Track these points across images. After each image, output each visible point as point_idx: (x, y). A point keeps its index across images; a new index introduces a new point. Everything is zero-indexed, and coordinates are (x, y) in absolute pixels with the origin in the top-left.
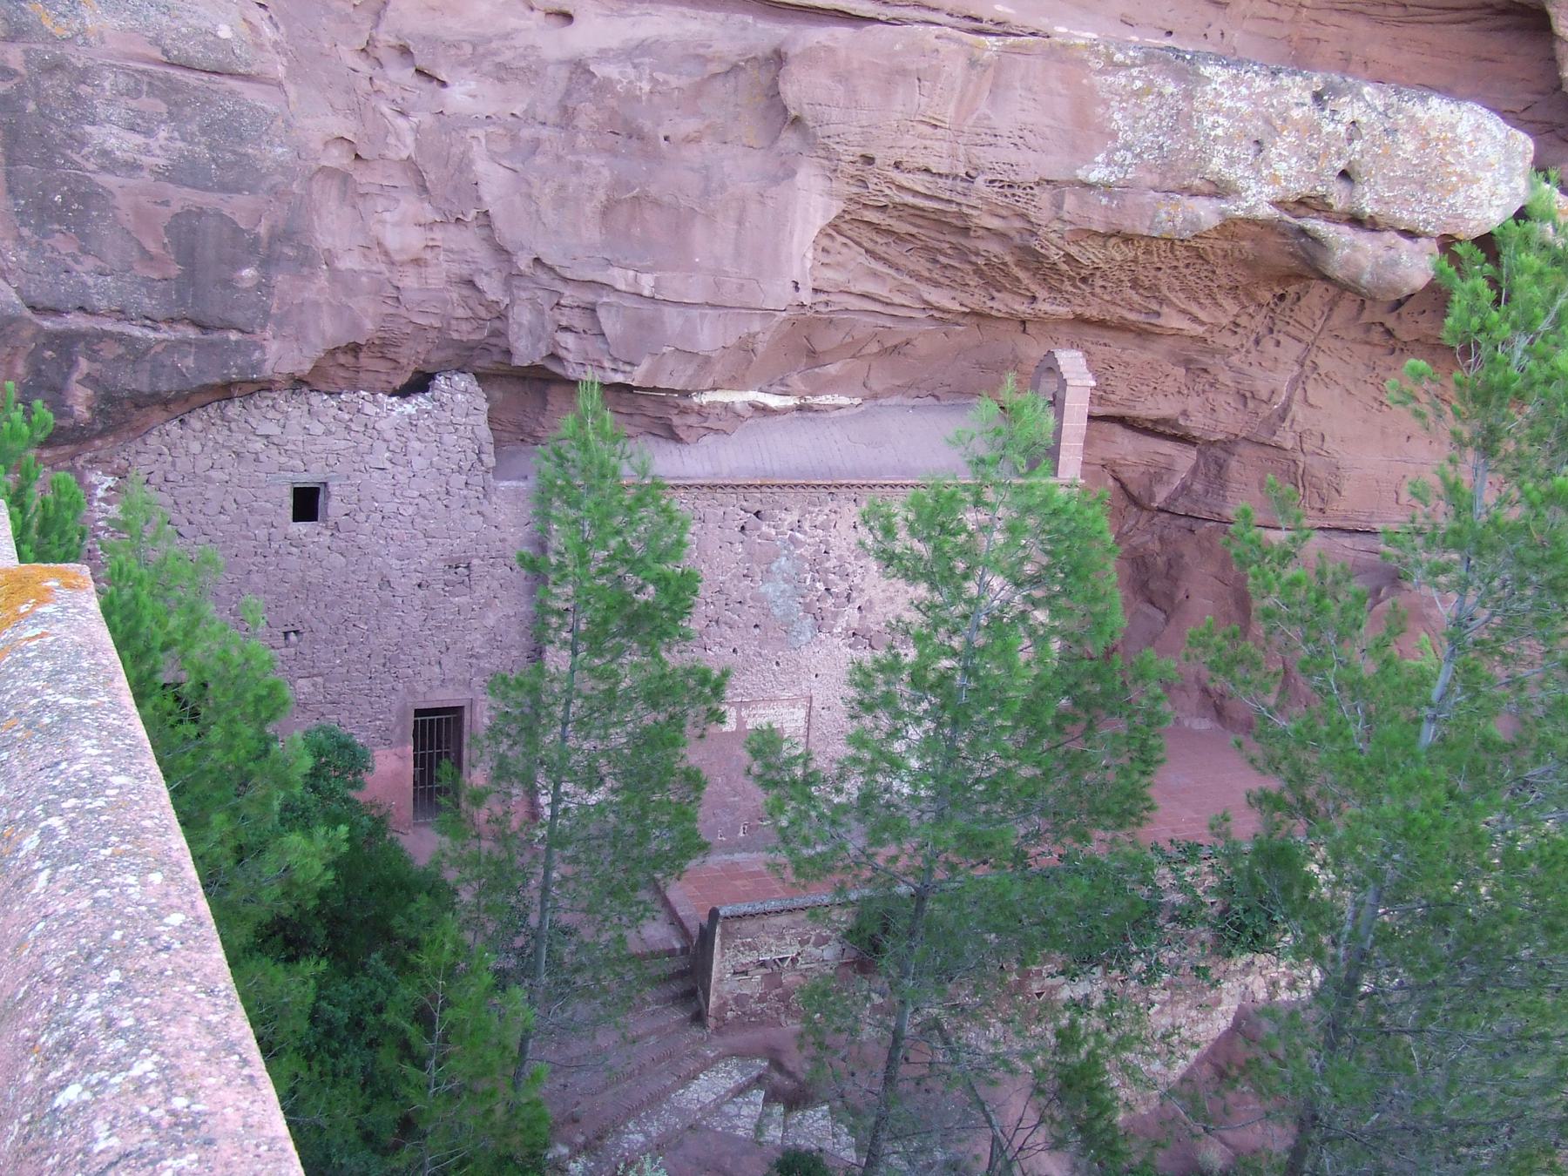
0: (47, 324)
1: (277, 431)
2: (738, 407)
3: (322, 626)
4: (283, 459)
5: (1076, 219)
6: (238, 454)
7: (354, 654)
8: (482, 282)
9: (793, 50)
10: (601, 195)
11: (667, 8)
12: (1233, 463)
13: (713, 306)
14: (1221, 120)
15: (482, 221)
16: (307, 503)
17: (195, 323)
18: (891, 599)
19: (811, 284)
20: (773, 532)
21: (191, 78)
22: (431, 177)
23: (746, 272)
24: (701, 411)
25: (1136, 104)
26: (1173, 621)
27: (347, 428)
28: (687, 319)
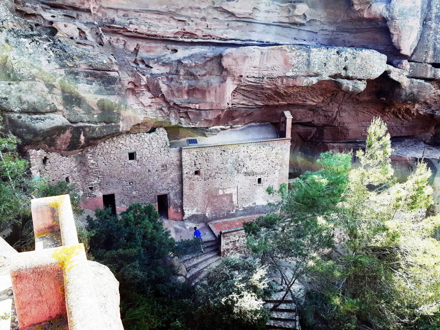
0: (74, 125)
1: (124, 142)
5: (286, 84)
6: (116, 148)
8: (164, 109)
10: (186, 89)
11: (197, 47)
13: (211, 110)
16: (132, 156)
17: (105, 122)
19: (231, 103)
21: (99, 72)
24: (211, 131)
27: (139, 140)
28: (206, 113)
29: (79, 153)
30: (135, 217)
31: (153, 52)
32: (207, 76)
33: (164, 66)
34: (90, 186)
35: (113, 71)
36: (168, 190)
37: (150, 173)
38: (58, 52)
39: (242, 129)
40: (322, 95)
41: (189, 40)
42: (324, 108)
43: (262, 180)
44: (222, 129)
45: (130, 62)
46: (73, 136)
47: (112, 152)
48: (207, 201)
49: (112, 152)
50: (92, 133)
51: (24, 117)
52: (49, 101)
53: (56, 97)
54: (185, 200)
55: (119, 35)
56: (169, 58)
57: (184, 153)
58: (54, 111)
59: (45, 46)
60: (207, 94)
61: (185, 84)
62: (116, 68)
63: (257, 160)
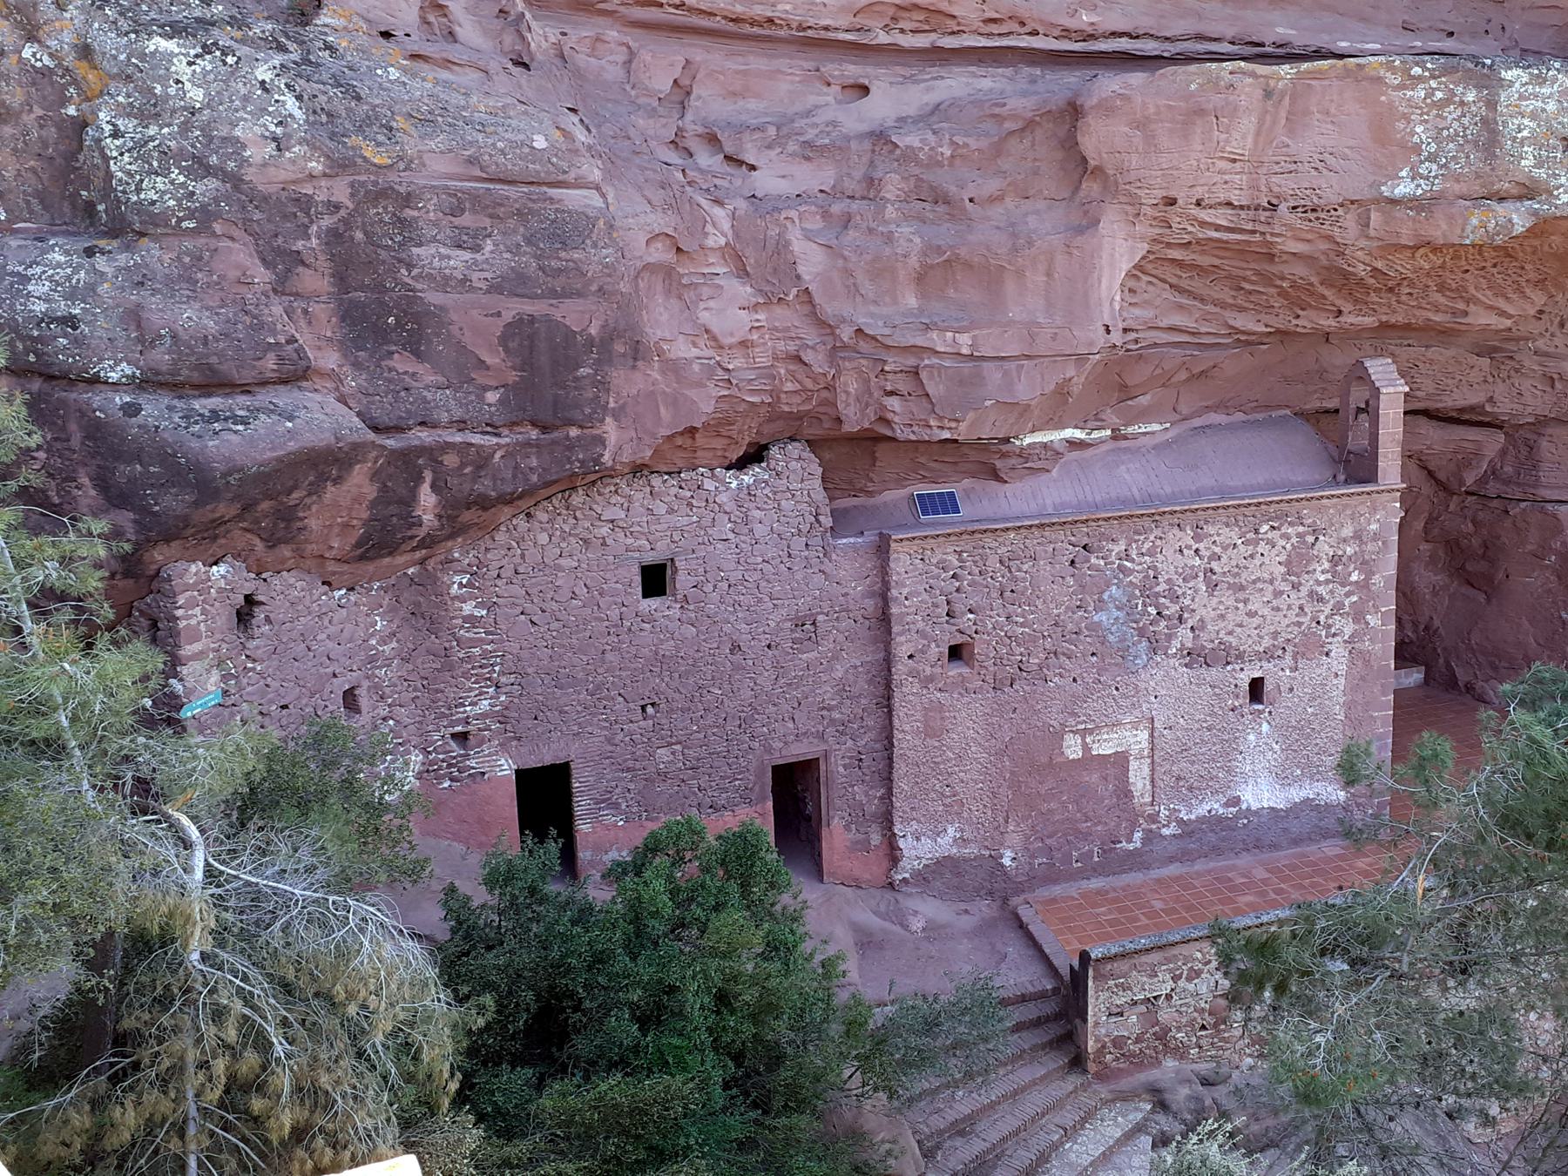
0: (391, 443)
2: (1056, 446)
3: (677, 696)
4: (630, 541)
7: (710, 720)
8: (808, 356)
9: (1090, 102)
10: (913, 261)
11: (956, 69)
12: (1544, 444)
13: (1028, 357)
14: (1526, 122)
15: (804, 298)
16: (655, 580)
18: (1222, 617)
19: (1121, 326)
20: (1102, 562)
22: (750, 263)
23: (1059, 321)
24: (1024, 454)
25: (1438, 116)
26: (1494, 601)
27: (690, 505)
28: (1006, 373)
29: (410, 571)
30: (674, 893)
31: (758, 96)
32: (1009, 202)
33: (808, 159)
34: (459, 729)
35: (578, 184)
36: (821, 736)
37: (738, 657)
38: (323, 98)
39: (1167, 444)
40: (1539, 284)
41: (922, 41)
42: (1540, 344)
43: (1269, 686)
44: (1073, 444)
45: (653, 144)
46: (384, 489)
47: (566, 562)
48: (1006, 793)
49: (566, 562)
50: (476, 477)
51: (154, 409)
52: (274, 333)
53: (305, 312)
54: (902, 785)
55: (601, 20)
56: (834, 123)
57: (902, 561)
58: (296, 374)
59: (263, 73)
60: (1010, 286)
61: (909, 239)
62: (593, 171)
63: (1242, 588)
